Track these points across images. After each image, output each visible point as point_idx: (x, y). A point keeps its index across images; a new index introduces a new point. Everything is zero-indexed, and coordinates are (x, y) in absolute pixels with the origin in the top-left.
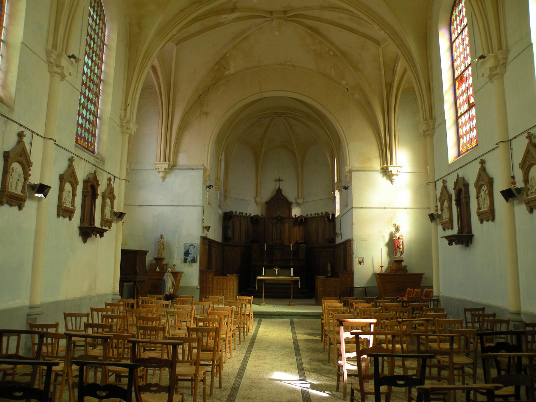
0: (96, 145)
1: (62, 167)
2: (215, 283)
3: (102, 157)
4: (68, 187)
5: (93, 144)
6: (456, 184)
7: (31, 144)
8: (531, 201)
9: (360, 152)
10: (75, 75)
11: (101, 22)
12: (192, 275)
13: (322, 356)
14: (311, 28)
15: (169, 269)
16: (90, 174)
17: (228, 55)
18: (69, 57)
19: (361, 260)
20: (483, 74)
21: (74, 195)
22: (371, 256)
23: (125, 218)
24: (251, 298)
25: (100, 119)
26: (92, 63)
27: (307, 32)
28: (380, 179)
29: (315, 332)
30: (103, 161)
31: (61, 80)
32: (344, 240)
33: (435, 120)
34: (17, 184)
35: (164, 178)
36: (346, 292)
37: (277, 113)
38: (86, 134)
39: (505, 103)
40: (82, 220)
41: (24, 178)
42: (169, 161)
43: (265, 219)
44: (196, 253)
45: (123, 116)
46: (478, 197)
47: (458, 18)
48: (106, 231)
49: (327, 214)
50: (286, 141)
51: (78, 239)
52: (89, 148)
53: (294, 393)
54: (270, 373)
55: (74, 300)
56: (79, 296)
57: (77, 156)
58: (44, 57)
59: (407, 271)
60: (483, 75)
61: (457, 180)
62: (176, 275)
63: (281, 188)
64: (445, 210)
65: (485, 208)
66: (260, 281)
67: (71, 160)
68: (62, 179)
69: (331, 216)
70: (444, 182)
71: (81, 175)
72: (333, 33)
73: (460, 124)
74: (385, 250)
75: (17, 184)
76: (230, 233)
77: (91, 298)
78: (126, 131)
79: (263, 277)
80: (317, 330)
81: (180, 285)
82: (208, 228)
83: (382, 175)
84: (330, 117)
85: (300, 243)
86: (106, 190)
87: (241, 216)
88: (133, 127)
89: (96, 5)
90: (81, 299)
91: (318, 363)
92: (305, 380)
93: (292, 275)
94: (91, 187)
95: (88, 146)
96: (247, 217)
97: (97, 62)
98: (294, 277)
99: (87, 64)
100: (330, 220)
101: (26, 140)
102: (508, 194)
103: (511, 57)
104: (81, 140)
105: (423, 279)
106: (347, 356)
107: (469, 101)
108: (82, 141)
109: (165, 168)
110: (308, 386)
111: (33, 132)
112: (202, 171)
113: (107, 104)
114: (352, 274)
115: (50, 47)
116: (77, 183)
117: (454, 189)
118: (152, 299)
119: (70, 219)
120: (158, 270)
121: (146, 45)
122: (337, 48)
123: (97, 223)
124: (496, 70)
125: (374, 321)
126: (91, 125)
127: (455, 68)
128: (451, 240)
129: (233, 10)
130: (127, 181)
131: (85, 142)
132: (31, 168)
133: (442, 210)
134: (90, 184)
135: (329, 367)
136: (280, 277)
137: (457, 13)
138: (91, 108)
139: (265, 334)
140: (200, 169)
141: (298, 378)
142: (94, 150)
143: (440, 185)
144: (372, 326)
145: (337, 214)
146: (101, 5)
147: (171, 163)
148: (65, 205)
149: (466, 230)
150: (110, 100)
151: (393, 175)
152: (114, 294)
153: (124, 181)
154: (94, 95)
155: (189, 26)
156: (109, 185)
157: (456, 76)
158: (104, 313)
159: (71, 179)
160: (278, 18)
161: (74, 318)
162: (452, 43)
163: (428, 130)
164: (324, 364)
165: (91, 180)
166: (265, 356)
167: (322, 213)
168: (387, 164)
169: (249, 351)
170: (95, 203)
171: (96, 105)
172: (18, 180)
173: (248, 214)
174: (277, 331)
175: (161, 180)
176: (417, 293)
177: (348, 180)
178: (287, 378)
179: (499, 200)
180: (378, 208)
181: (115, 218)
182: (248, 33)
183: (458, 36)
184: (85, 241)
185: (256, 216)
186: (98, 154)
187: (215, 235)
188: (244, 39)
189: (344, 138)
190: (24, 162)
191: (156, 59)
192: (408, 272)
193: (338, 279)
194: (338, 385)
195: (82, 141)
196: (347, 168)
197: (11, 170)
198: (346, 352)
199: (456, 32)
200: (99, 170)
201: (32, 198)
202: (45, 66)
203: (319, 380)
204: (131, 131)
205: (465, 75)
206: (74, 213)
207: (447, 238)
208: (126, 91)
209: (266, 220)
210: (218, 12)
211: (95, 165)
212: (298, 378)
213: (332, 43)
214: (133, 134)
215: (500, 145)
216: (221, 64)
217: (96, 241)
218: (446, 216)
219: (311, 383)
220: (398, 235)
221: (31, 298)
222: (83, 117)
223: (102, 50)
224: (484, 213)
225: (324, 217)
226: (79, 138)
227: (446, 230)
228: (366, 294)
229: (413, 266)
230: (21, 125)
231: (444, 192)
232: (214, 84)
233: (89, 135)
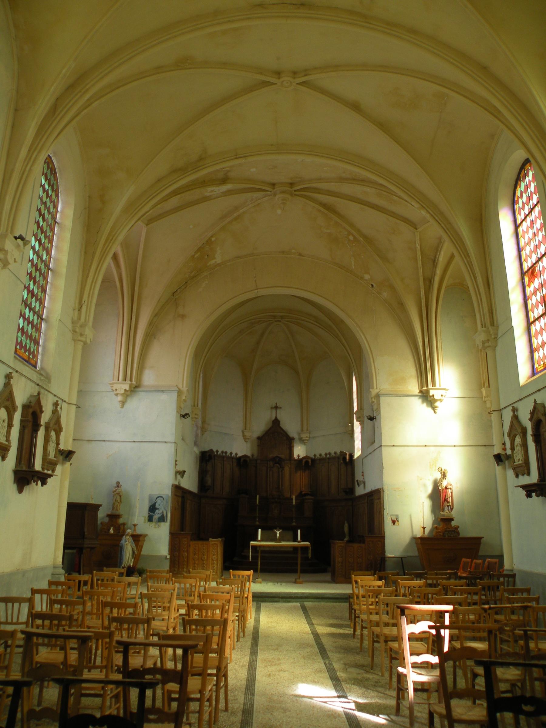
0: (40, 357)
2: (191, 550)
3: (47, 374)
5: (35, 356)
6: (532, 413)
9: (391, 369)
11: (54, 193)
12: (159, 539)
13: (359, 659)
14: (324, 205)
15: (129, 530)
16: (31, 396)
17: (213, 239)
18: (16, 238)
19: (394, 518)
22: (409, 514)
23: (75, 457)
24: (250, 573)
25: (46, 321)
26: (39, 246)
27: (319, 211)
28: (418, 406)
29: (340, 622)
30: (48, 378)
32: (368, 490)
33: (498, 326)
35: (123, 403)
36: (377, 564)
37: (274, 317)
38: (28, 341)
40: (19, 460)
42: (131, 380)
43: (256, 460)
44: (166, 508)
45: (76, 318)
47: (524, 196)
48: (50, 476)
49: (343, 454)
50: (287, 352)
53: (335, 717)
54: (293, 686)
57: (17, 371)
59: (458, 533)
61: (535, 408)
62: (138, 539)
63: (279, 418)
64: (518, 449)
66: (255, 547)
67: (8, 377)
69: (348, 457)
70: (515, 410)
71: (20, 399)
72: (353, 211)
73: (533, 333)
74: (427, 504)
76: (209, 480)
77: (24, 573)
78: (80, 338)
79: (260, 541)
80: (341, 619)
81: (143, 553)
82: (182, 473)
83: (420, 401)
84: (349, 322)
85: (306, 495)
86: (51, 419)
87: (224, 457)
88: (89, 332)
89: (49, 172)
90: (11, 574)
91: (358, 671)
92: (346, 697)
93: (299, 539)
94: (32, 415)
95: (29, 358)
96: (233, 458)
97: (46, 245)
98: (303, 543)
100: (347, 462)
104: (21, 349)
105: (482, 546)
106: (413, 661)
109: (125, 390)
110: (353, 706)
111: (62, 400)
112: (176, 394)
113: (57, 302)
114: (382, 538)
116: (15, 409)
117: (530, 420)
118: (107, 573)
120: (112, 531)
121: (111, 224)
122: (359, 231)
123: (38, 467)
125: (450, 608)
126: (34, 330)
127: (523, 259)
128: (529, 490)
129: (224, 180)
130: (78, 407)
133: (513, 449)
134: (31, 410)
135: (375, 676)
136: (283, 543)
137: (522, 188)
138: (35, 306)
139: (270, 625)
140: (172, 391)
141: (334, 693)
142: (36, 363)
143: (508, 415)
144: (447, 615)
145: (357, 453)
146: (55, 173)
147: (134, 383)
151: (436, 401)
152: (55, 567)
154: (40, 290)
155: (166, 200)
156: (55, 412)
157: (525, 269)
160: (283, 192)
161: (10, 605)
162: (517, 227)
163: (488, 340)
164: (367, 672)
165: (33, 404)
166: (279, 659)
167: (335, 453)
168: (427, 386)
169: (254, 652)
170: (36, 438)
171: (41, 302)
173: (234, 454)
174: (286, 621)
175: (119, 405)
176: (477, 565)
177: (375, 407)
178: (317, 693)
180: (417, 446)
182: (241, 211)
183: (525, 218)
184: (20, 491)
185: (245, 456)
186: (42, 368)
187: (190, 483)
188: (236, 219)
189: (369, 351)
192: (461, 535)
193: (363, 545)
194: (398, 705)
195: (23, 350)
196: (374, 392)
198: (411, 655)
199: (522, 212)
200: (42, 391)
203: (366, 697)
204: (86, 338)
205: (538, 268)
206: (9, 450)
207: (524, 487)
208: (82, 285)
209: (259, 462)
210: (204, 183)
211: (38, 385)
212: (335, 694)
213: (352, 225)
216: (204, 251)
217: (36, 490)
218: (519, 457)
219: (355, 702)
220: (444, 483)
222: (24, 319)
223: (52, 230)
224: (519, 466)
225: (338, 458)
226: (18, 347)
227: (520, 476)
228: (404, 566)
229: (467, 525)
231: (515, 423)
232: (193, 277)
233: (31, 343)
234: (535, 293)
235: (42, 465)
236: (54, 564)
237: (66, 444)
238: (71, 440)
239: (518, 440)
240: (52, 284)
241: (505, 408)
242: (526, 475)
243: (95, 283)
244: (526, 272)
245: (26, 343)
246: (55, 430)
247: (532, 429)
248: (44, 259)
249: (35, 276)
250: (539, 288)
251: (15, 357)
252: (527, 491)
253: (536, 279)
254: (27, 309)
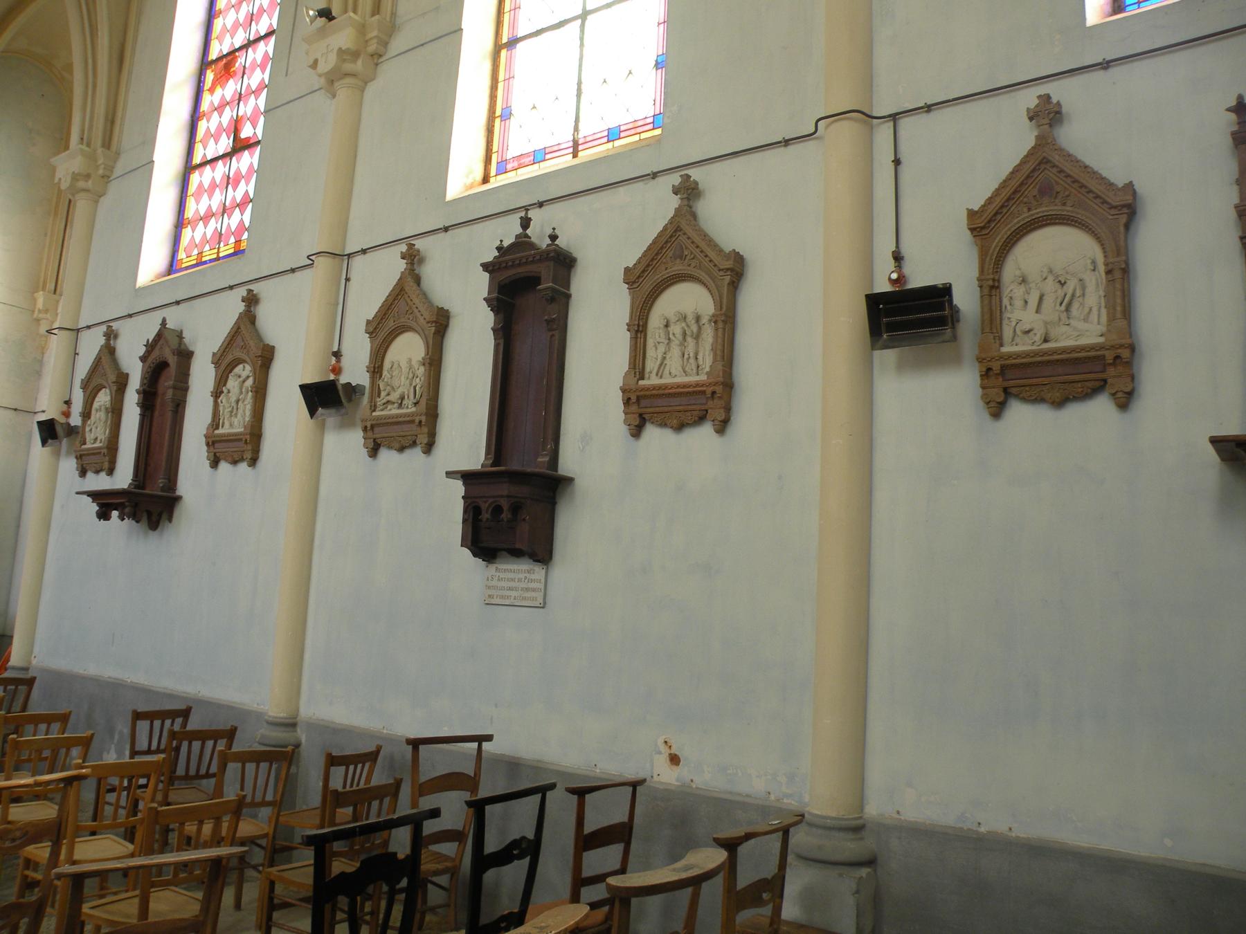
6: (151, 347)
8: (379, 425)
20: (316, 61)
33: (118, 154)
39: (355, 156)
46: (217, 394)
60: (314, 65)
61: (159, 336)
65: (235, 425)
70: (111, 335)
102: (323, 396)
103: (398, 44)
107: (237, 131)
117: (143, 359)
124: (355, 61)
127: (214, 35)
128: (106, 503)
133: (86, 415)
143: (91, 345)
149: (161, 482)
157: (213, 55)
163: (88, 176)
179: (285, 408)
205: (240, 61)
207: (95, 495)
215: (321, 262)
218: (96, 434)
224: (94, 453)
231: (106, 360)
234: (220, 109)
239: (103, 398)
241: (88, 327)
242: (103, 474)
244: (213, 62)
247: (143, 378)
250: (232, 101)
252: (101, 506)
253: (231, 82)
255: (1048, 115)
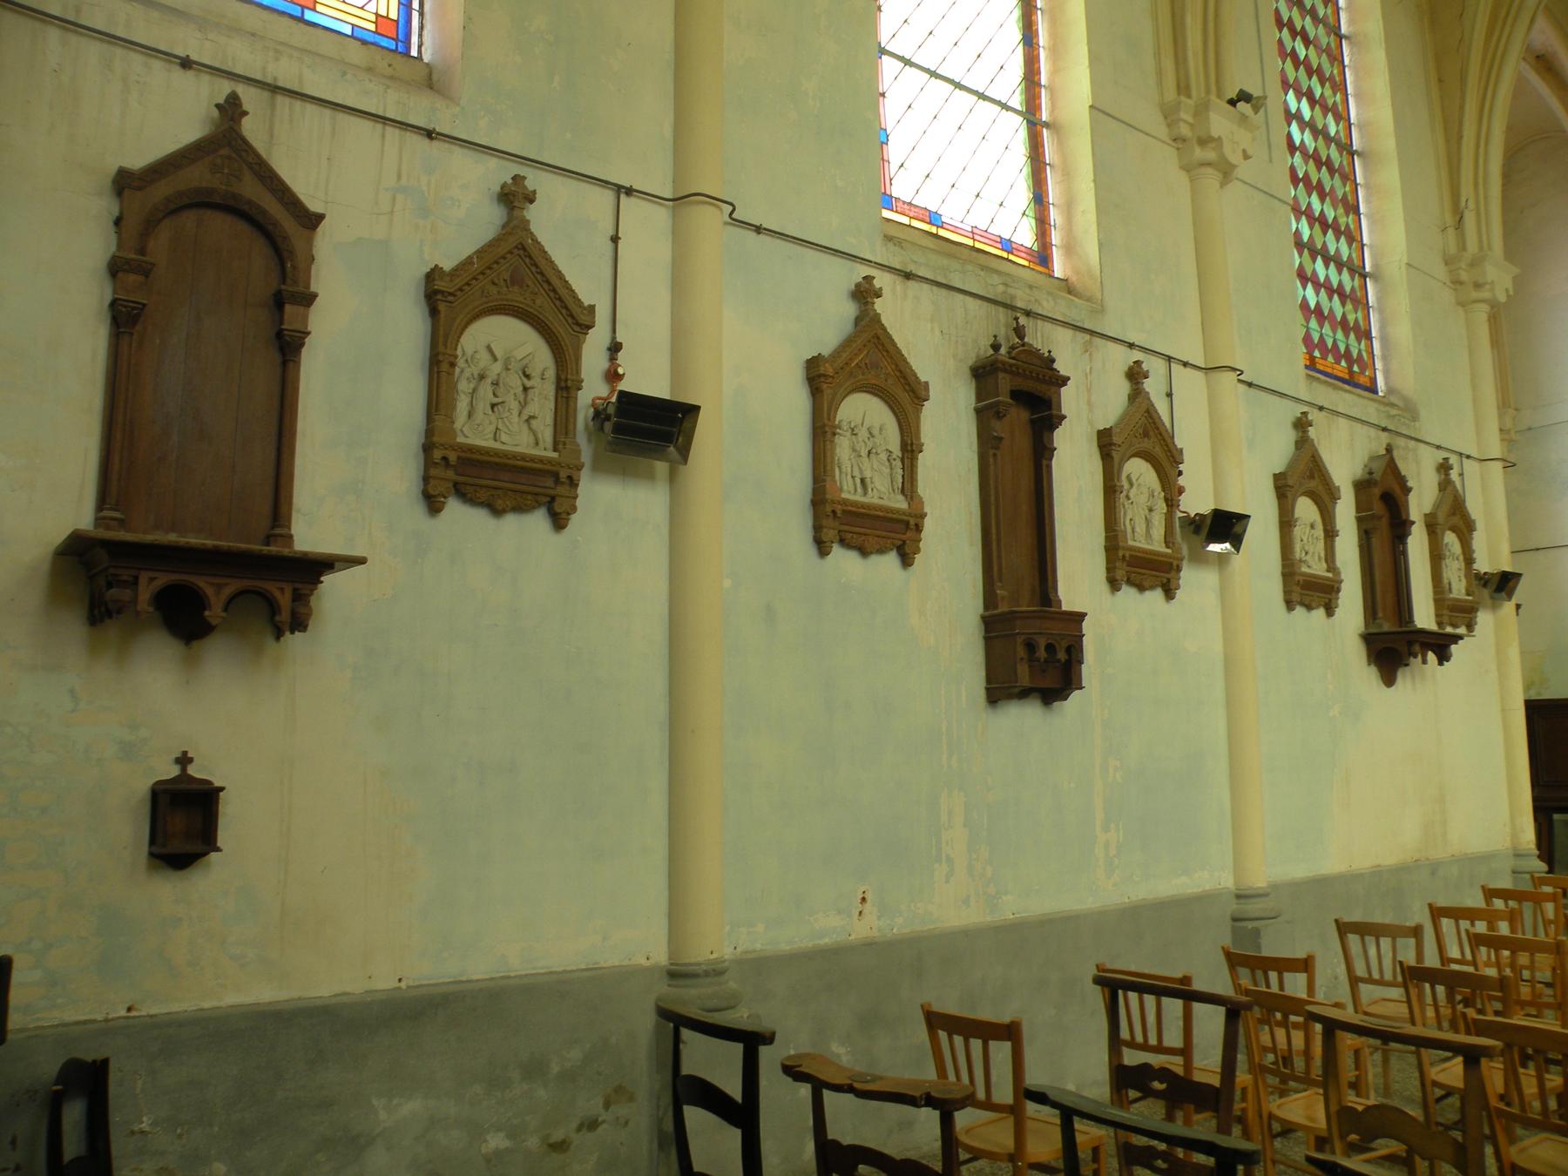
0: (1379, 365)
1: (1278, 450)
3: (1405, 399)
4: (1305, 509)
5: (1366, 363)
7: (1170, 395)
10: (1262, 153)
16: (1373, 458)
18: (1233, 103)
21: (1330, 534)
23: (1522, 591)
26: (1312, 108)
30: (1410, 411)
31: (1223, 185)
34: (1148, 521)
38: (1340, 335)
41: (1166, 500)
45: (1453, 249)
48: (1456, 638)
51: (1369, 676)
52: (1357, 379)
55: (1377, 873)
56: (1390, 859)
57: (1321, 408)
58: (1162, 131)
67: (1301, 424)
68: (1284, 488)
71: (1343, 468)
75: (1148, 521)
77: (1434, 868)
78: (1475, 295)
86: (1437, 506)
90: (1402, 870)
94: (1384, 502)
95: (1351, 373)
99: (1298, 116)
101: (1154, 387)
104: (1324, 357)
108: (1330, 359)
111: (1169, 359)
113: (1389, 228)
115: (1171, 94)
116: (1333, 494)
119: (1330, 611)
123: (1424, 616)
130: (1509, 465)
131: (1341, 363)
132: (1181, 467)
134: (1377, 491)
142: (1374, 380)
148: (1304, 569)
150: (1395, 208)
152: (1517, 856)
153: (1499, 465)
156: (1445, 485)
158: (1481, 927)
159: (1312, 484)
165: (1377, 476)
170: (1404, 553)
171: (1353, 237)
172: (1151, 510)
181: (1486, 593)
184: (1389, 680)
186: (1390, 391)
190: (1158, 451)
191: (1542, 23)
195: (1330, 359)
197: (1126, 486)
200: (1401, 442)
201: (1200, 558)
202: (1167, 158)
206: (1338, 590)
211: (1384, 429)
214: (1502, 298)
217: (1428, 678)
221: (1238, 867)
226: (1317, 354)
230: (1131, 346)
233: (1347, 336)
235: (1437, 616)
236: (1515, 848)
237: (1491, 555)
238: (1505, 549)
240: (1367, 186)
243: (1487, 144)
245: (1335, 342)
246: (1453, 529)
248: (1332, 133)
249: (1319, 181)
251: (1308, 376)
254: (1319, 261)
255: (514, 197)
